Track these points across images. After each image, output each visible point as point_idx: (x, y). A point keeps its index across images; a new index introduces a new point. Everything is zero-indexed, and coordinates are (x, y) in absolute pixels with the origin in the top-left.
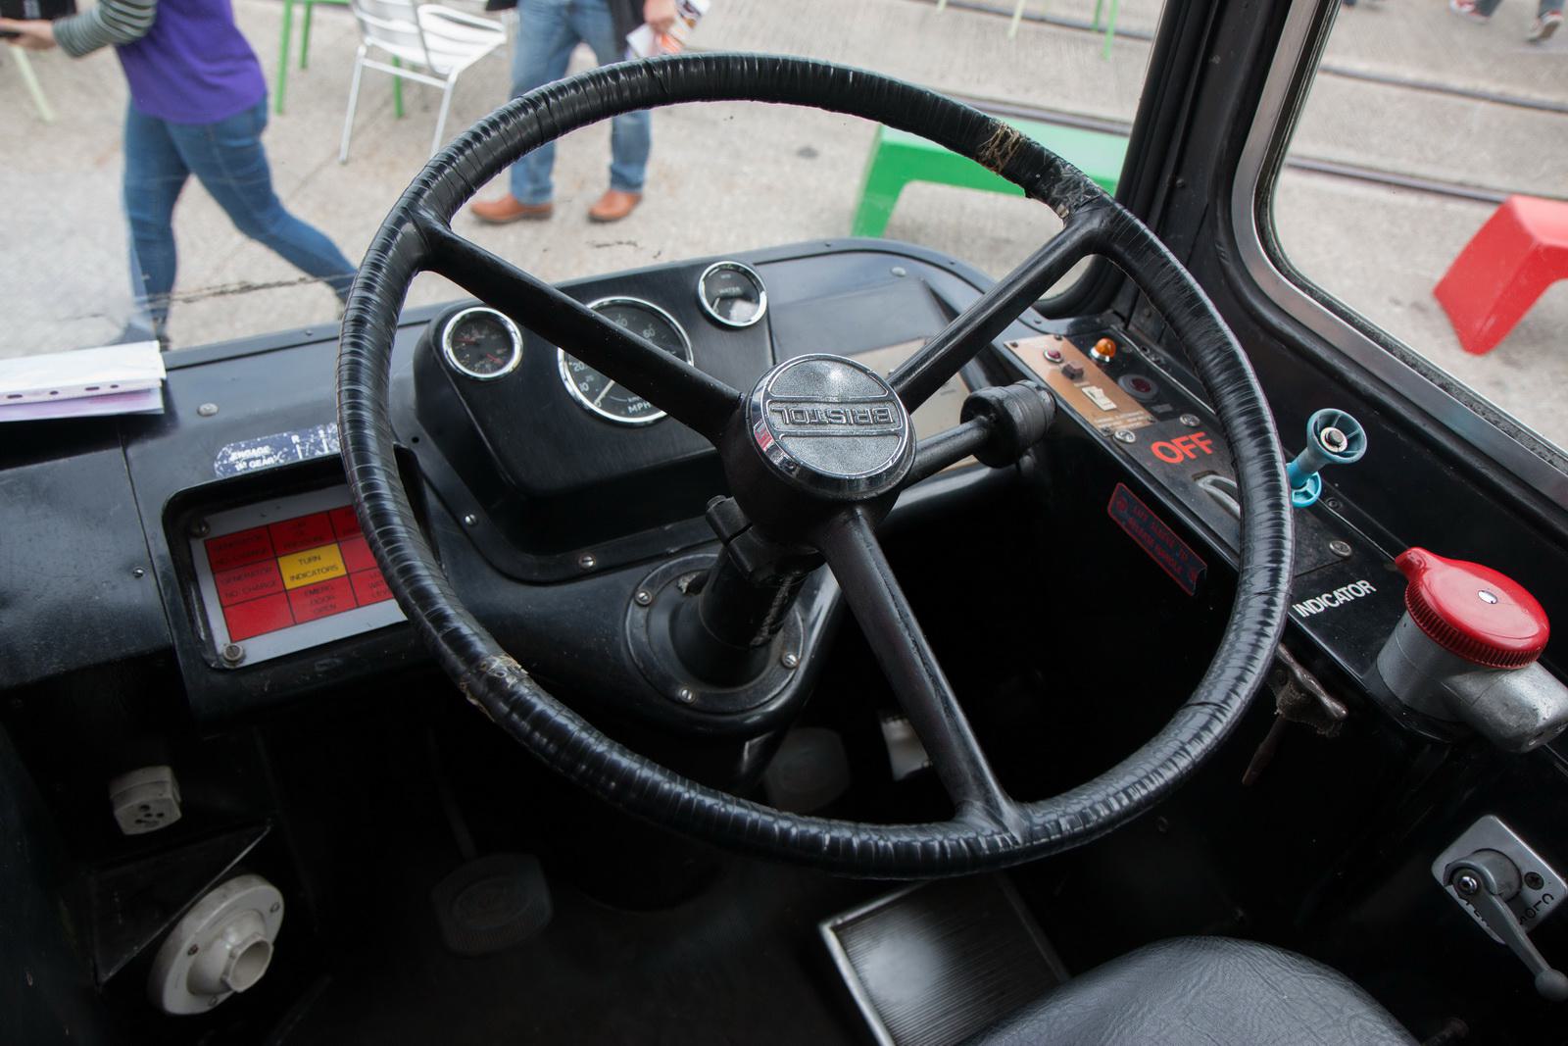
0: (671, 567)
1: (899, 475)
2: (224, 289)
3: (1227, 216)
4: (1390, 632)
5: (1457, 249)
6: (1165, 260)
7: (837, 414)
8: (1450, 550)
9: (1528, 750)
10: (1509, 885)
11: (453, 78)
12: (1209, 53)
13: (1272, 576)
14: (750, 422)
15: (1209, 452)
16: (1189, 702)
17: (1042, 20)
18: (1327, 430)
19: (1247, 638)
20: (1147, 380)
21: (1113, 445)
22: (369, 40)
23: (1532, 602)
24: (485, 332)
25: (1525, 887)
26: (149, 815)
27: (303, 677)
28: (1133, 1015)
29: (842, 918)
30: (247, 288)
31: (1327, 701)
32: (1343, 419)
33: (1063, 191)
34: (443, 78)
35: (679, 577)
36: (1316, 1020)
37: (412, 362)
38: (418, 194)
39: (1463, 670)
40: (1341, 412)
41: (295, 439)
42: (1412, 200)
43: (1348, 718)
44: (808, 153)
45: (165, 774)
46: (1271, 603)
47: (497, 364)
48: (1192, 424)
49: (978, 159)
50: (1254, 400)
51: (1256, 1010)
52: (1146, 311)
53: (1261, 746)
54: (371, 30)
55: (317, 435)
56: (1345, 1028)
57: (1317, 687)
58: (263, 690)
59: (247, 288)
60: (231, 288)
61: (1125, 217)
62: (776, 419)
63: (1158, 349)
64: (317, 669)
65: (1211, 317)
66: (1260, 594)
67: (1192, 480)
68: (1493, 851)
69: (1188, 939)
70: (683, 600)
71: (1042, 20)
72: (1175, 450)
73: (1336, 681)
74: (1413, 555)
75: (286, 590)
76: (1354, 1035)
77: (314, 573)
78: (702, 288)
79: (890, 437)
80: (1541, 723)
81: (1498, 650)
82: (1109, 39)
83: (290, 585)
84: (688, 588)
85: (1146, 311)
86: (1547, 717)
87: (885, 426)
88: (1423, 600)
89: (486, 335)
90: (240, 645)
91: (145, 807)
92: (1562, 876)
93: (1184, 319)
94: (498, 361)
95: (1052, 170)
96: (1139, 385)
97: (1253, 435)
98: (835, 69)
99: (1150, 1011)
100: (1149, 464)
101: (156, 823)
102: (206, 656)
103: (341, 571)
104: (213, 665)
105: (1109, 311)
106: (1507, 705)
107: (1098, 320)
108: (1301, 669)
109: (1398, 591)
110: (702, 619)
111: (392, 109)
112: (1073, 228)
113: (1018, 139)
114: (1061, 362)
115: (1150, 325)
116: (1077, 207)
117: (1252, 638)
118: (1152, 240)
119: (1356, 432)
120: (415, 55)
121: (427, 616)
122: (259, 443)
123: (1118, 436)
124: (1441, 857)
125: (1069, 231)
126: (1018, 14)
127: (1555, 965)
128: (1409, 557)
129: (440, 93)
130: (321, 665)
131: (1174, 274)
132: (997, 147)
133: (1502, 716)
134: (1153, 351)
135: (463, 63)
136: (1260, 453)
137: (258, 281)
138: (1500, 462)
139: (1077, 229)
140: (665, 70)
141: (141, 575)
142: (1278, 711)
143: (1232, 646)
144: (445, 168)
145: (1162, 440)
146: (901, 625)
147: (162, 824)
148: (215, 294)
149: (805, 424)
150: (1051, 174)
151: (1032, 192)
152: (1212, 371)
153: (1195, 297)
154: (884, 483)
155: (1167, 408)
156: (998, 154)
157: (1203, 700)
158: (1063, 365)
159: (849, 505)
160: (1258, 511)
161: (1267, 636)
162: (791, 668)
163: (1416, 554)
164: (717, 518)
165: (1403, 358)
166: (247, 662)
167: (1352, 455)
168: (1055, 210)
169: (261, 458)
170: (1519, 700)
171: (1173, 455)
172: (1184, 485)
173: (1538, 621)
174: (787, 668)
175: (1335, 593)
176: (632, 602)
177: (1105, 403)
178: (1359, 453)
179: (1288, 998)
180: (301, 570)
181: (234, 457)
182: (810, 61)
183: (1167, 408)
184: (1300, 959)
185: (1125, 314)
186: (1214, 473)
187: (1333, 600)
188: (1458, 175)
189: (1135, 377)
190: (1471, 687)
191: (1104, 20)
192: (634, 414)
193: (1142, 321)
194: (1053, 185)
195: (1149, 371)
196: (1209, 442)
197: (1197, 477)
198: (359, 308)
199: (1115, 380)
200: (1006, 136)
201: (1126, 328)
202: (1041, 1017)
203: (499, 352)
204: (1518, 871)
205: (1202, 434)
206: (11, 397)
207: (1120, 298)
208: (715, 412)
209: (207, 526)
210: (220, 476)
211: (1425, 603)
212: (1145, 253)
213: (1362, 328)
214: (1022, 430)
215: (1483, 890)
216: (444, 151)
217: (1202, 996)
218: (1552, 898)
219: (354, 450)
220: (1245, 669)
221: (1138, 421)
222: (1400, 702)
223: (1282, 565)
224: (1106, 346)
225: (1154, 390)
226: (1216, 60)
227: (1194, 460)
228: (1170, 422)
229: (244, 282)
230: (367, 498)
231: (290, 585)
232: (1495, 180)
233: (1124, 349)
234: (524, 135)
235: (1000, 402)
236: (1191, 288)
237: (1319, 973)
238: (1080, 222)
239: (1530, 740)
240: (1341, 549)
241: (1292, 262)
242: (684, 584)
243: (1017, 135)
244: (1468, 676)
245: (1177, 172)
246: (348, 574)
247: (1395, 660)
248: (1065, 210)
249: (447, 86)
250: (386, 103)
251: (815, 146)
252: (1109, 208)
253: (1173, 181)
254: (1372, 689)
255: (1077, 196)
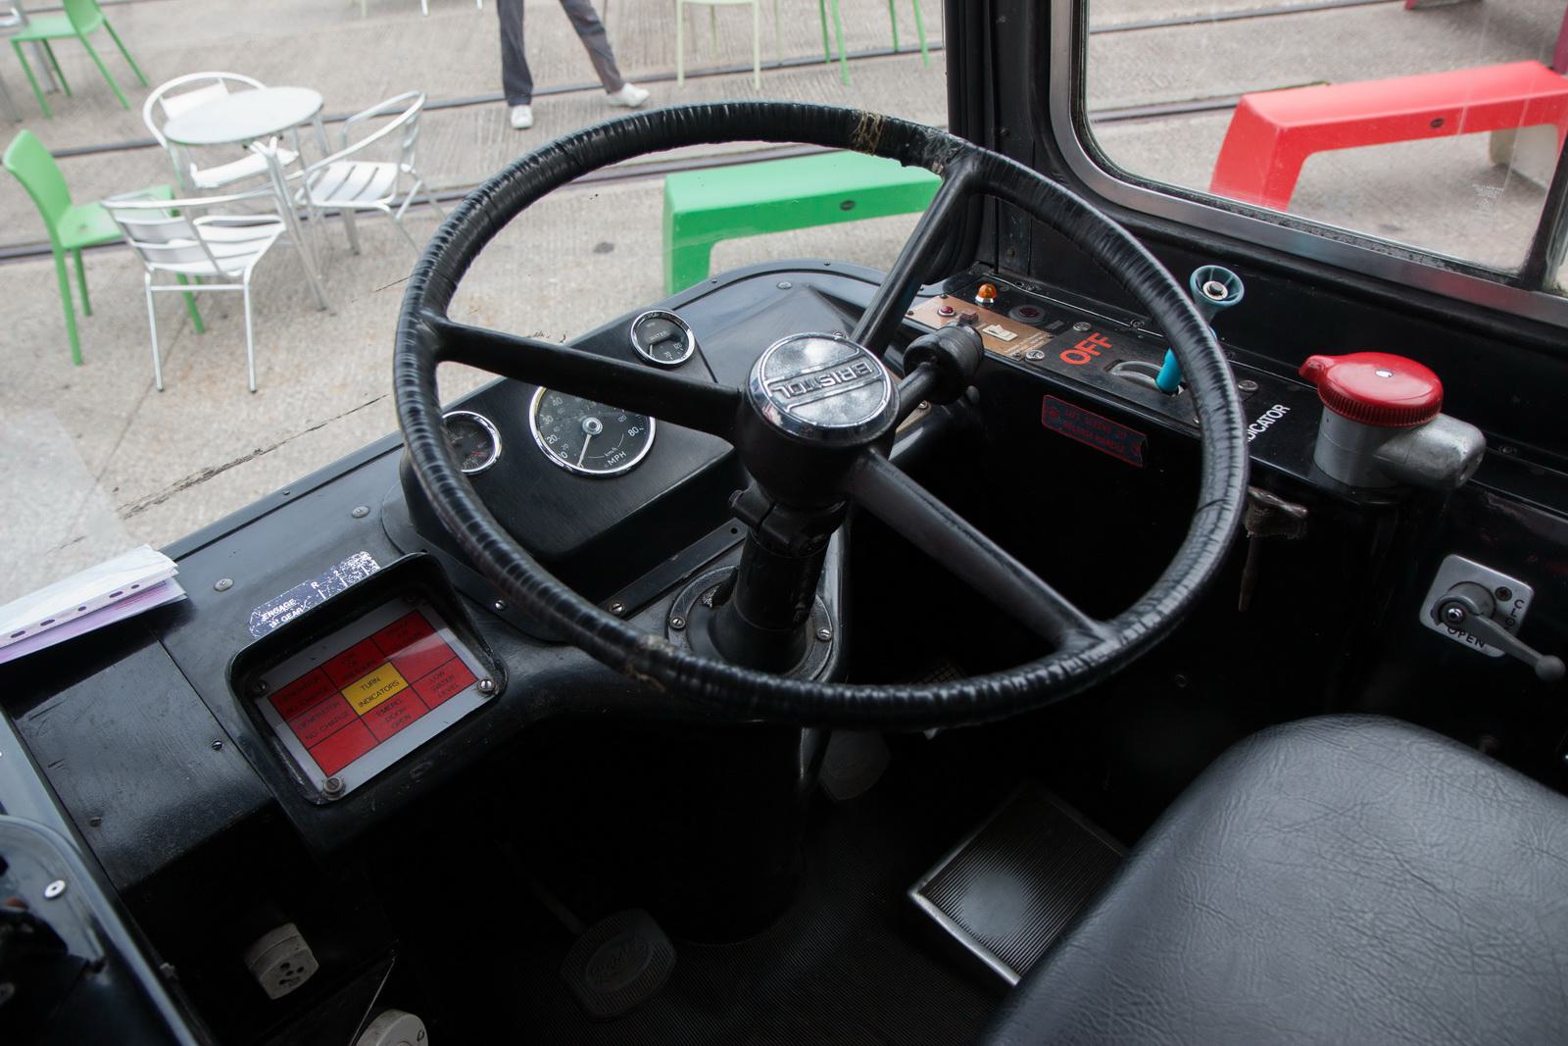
0: (691, 589)
1: (893, 412)
2: (189, 481)
3: (1054, 146)
4: (1315, 436)
5: (1214, 157)
6: (1036, 181)
7: (821, 385)
8: (1341, 349)
9: (1461, 484)
10: (1485, 604)
11: (247, 279)
12: (994, 17)
13: (1221, 393)
14: (757, 407)
15: (1109, 346)
16: (1199, 506)
17: (780, 67)
18: (1206, 286)
19: (1222, 445)
20: (1034, 307)
21: (1027, 365)
22: (152, 266)
23: (1422, 369)
24: (462, 432)
25: (1499, 602)
26: (290, 973)
27: (402, 788)
28: (1236, 806)
29: (925, 880)
30: (210, 474)
31: (1287, 507)
32: (1216, 270)
33: (933, 151)
34: (239, 280)
35: (701, 596)
36: (1383, 756)
37: (399, 481)
38: (417, 298)
39: (1387, 438)
40: (1213, 267)
41: (314, 585)
42: (1158, 125)
43: (1310, 513)
44: (605, 248)
45: (292, 930)
46: (1229, 412)
47: (481, 458)
48: (1086, 329)
49: (853, 147)
50: (1151, 266)
51: (1333, 766)
52: (1009, 252)
53: (1245, 572)
54: (150, 255)
55: (333, 575)
56: (1408, 755)
57: (1276, 499)
58: (372, 811)
59: (210, 474)
60: (196, 478)
61: (990, 157)
62: (779, 397)
63: (1030, 280)
64: (414, 776)
65: (1090, 213)
66: (1218, 409)
67: (1104, 372)
68: (1468, 581)
69: (1254, 736)
70: (713, 613)
71: (780, 67)
72: (1081, 353)
73: (1289, 489)
74: (1312, 363)
75: (359, 717)
76: (1416, 757)
77: (379, 694)
78: (634, 338)
79: (875, 384)
80: (1463, 457)
81: (1409, 410)
82: (845, 64)
83: (360, 711)
84: (713, 602)
85: (1009, 252)
86: (1466, 451)
87: (867, 376)
88: (1335, 392)
89: (464, 435)
90: (337, 776)
91: (285, 966)
92: (1523, 581)
93: (1069, 224)
94: (483, 454)
95: (917, 137)
96: (1028, 313)
97: (1161, 294)
98: (711, 107)
99: (1248, 797)
100: (1065, 370)
101: (298, 979)
102: (308, 797)
103: (403, 684)
104: (318, 803)
105: (976, 263)
106: (1431, 453)
107: (970, 273)
108: (1256, 490)
109: (1311, 400)
110: (742, 616)
111: (192, 325)
112: (952, 178)
113: (881, 120)
114: (955, 314)
115: (1017, 262)
116: (948, 161)
117: (1226, 444)
118: (1019, 169)
119: (1230, 279)
120: (204, 267)
121: (577, 623)
122: (282, 599)
123: (1030, 357)
124: (1423, 608)
125: (949, 181)
126: (757, 68)
127: (1544, 652)
128: (1309, 365)
129: (241, 293)
130: (415, 771)
131: (1046, 190)
132: (866, 131)
133: (1430, 463)
134: (1027, 283)
135: (253, 260)
136: (1172, 305)
137: (220, 462)
138: (1349, 268)
139: (956, 177)
140: (573, 144)
141: (221, 746)
142: (1249, 533)
143: (1213, 455)
144: (428, 272)
145: (1067, 349)
146: (948, 524)
147: (304, 978)
148: (182, 488)
149: (803, 394)
150: (918, 140)
151: (906, 161)
152: (1108, 255)
153: (1071, 202)
154: (886, 420)
155: (1059, 324)
156: (868, 137)
157: (1208, 501)
158: (958, 317)
159: (862, 449)
160: (1188, 350)
161: (1236, 437)
162: (828, 641)
163: (1316, 361)
164: (742, 510)
165: (1241, 213)
166: (349, 790)
167: (1233, 298)
168: (930, 169)
169: (289, 611)
170: (1440, 446)
171: (1081, 358)
172: (1100, 378)
173: (1429, 382)
174: (825, 641)
175: (1258, 421)
176: (670, 630)
177: (1006, 335)
178: (1240, 295)
179: (1354, 748)
180: (366, 694)
181: (264, 618)
182: (689, 106)
183: (1059, 324)
184: (1350, 717)
185: (993, 261)
186: (1121, 361)
187: (1259, 427)
188: (1189, 94)
189: (1021, 307)
190: (1397, 450)
191: (834, 50)
192: (615, 465)
193: (1008, 261)
194: (922, 149)
195: (1029, 299)
196: (1106, 338)
197: (1108, 369)
198: (409, 402)
199: (1007, 316)
200: (870, 120)
201: (996, 272)
202: (1163, 836)
203: (479, 446)
204: (1488, 591)
205: (1097, 334)
206: (44, 624)
207: (981, 250)
208: (723, 411)
209: (266, 684)
210: (258, 637)
211: (1338, 394)
212: (1017, 179)
213: (1199, 200)
214: (963, 364)
215: (1469, 614)
216: (422, 259)
217: (1285, 772)
218: (1523, 602)
219: (457, 513)
220: (1231, 467)
221: (1040, 341)
222: (1347, 486)
223: (1225, 382)
224: (987, 290)
225: (1042, 313)
226: (1002, 19)
227: (1100, 356)
228: (1066, 333)
229: (207, 469)
230: (485, 547)
231: (360, 711)
232: (1224, 89)
233: (1002, 289)
234: (480, 229)
235: (936, 344)
236: (1066, 196)
237: (1369, 722)
238: (956, 171)
239: (1459, 477)
240: (1249, 386)
241: (1122, 167)
242: (709, 601)
243: (879, 118)
244: (1393, 441)
245: (998, 123)
246: (410, 685)
247: (1329, 453)
248: (938, 167)
249: (245, 287)
250: (184, 323)
251: (609, 240)
252: (975, 153)
253: (997, 132)
254: (1320, 482)
255: (945, 151)
